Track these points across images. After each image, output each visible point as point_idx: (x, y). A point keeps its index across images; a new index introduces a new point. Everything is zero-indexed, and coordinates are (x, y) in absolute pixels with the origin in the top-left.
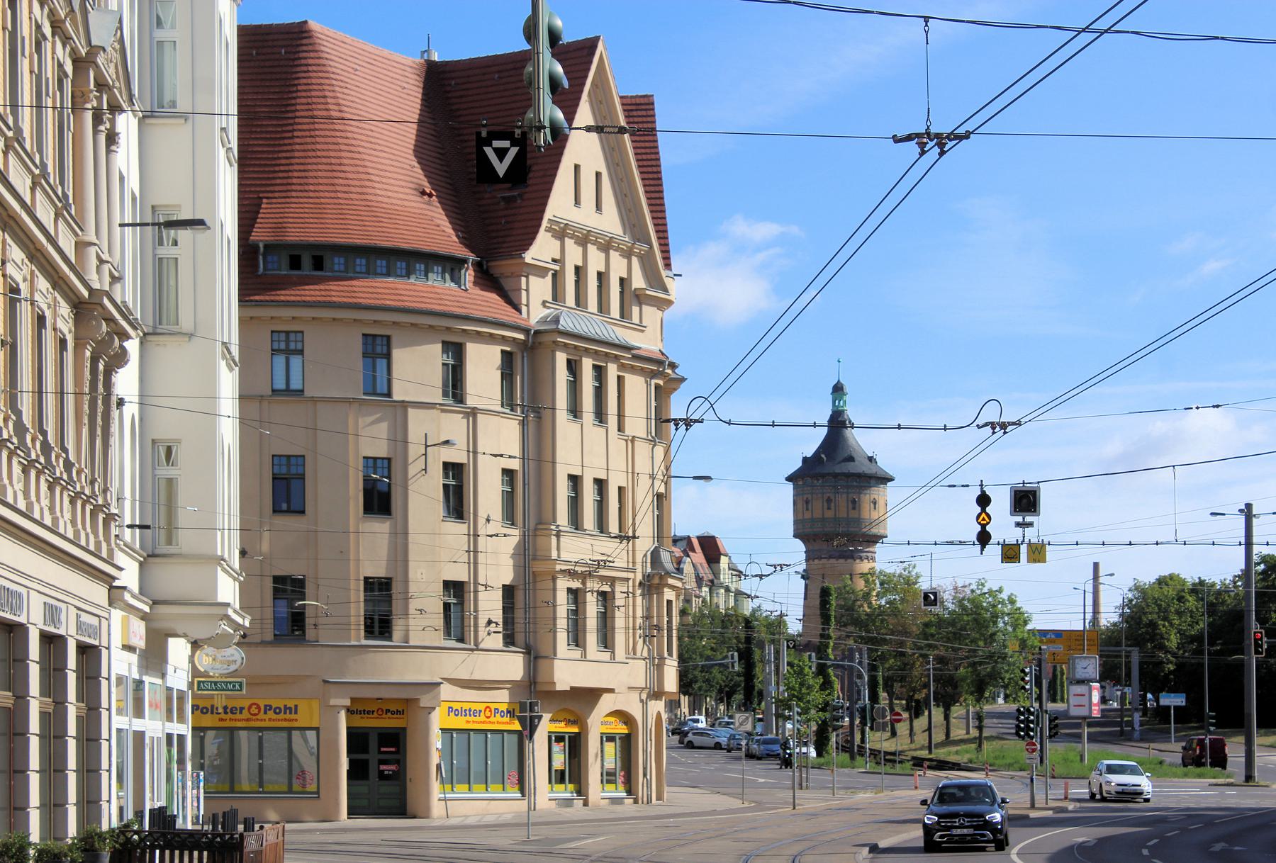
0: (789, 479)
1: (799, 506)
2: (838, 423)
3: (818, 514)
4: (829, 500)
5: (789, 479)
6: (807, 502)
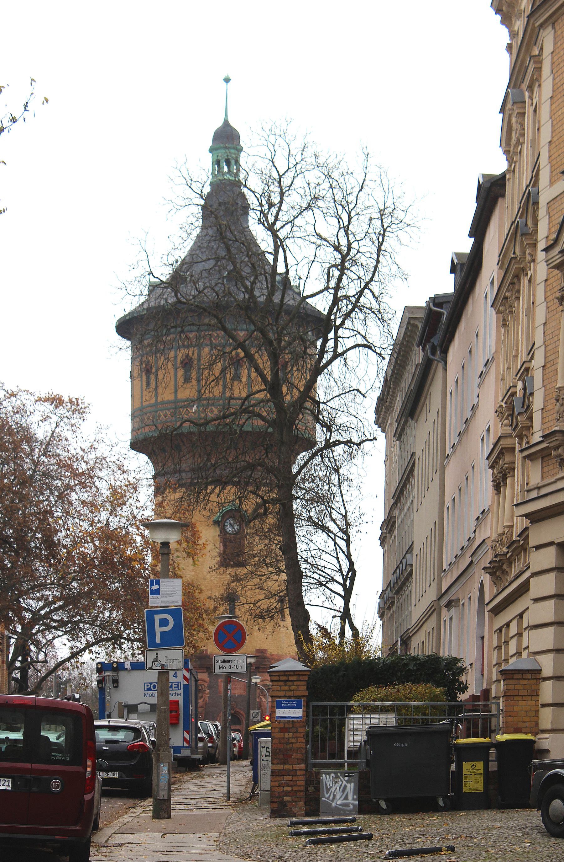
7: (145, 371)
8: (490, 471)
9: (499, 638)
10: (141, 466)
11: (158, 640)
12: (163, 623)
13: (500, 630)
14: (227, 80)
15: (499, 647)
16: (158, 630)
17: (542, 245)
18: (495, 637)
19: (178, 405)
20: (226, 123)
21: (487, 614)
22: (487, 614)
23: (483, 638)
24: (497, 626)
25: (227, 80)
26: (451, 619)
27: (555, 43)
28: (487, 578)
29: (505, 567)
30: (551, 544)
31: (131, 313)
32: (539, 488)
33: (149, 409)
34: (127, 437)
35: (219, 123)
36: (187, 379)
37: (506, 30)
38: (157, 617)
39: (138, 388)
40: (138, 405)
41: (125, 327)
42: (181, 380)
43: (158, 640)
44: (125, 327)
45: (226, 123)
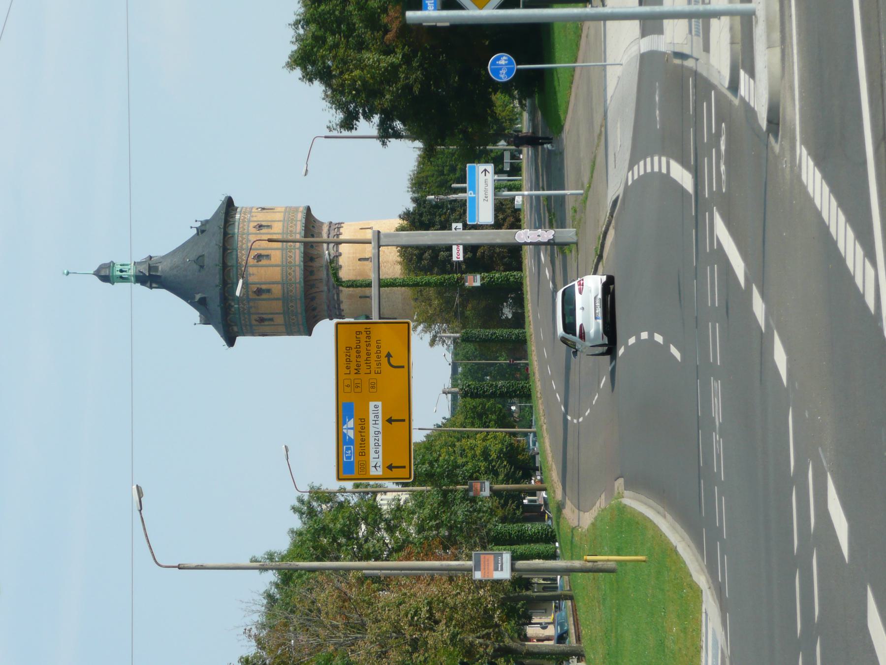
0: (231, 342)
1: (267, 329)
2: (150, 276)
5: (231, 342)
6: (262, 320)
14: (68, 273)
34: (305, 338)
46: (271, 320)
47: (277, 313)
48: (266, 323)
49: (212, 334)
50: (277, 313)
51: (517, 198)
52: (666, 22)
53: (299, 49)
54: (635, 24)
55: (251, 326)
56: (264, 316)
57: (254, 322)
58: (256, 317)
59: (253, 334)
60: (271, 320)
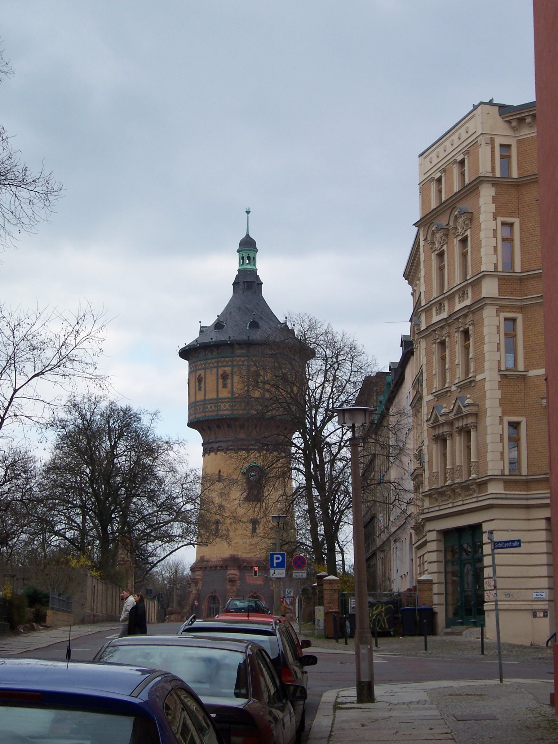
0: (185, 353)
1: (192, 384)
2: (248, 284)
3: (212, 395)
4: (225, 377)
5: (185, 353)
6: (200, 380)
7: (196, 382)
8: (412, 482)
9: (420, 561)
10: (195, 439)
11: (275, 565)
12: (277, 558)
13: (420, 557)
14: (248, 212)
15: (420, 565)
16: (275, 561)
17: (425, 418)
18: (418, 560)
19: (217, 401)
20: (248, 236)
21: (414, 549)
22: (414, 549)
23: (412, 560)
24: (419, 555)
25: (248, 212)
26: (396, 548)
27: (426, 346)
28: (413, 532)
29: (421, 528)
30: (434, 530)
31: (189, 346)
32: (428, 508)
33: (200, 403)
34: (185, 419)
35: (244, 236)
36: (225, 386)
37: (409, 289)
38: (275, 556)
39: (193, 391)
40: (193, 400)
41: (186, 353)
42: (220, 386)
43: (275, 565)
44: (186, 353)
45: (248, 236)
46: (200, 388)
47: (205, 395)
48: (197, 384)
49: (191, 336)
50: (205, 395)
51: (428, 505)
52: (512, 355)
53: (245, 340)
54: (502, 469)
55: (196, 370)
56: (203, 383)
57: (198, 373)
58: (203, 375)
59: (190, 373)
60: (200, 388)
